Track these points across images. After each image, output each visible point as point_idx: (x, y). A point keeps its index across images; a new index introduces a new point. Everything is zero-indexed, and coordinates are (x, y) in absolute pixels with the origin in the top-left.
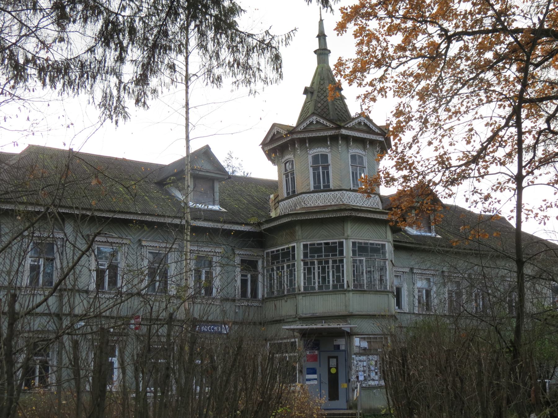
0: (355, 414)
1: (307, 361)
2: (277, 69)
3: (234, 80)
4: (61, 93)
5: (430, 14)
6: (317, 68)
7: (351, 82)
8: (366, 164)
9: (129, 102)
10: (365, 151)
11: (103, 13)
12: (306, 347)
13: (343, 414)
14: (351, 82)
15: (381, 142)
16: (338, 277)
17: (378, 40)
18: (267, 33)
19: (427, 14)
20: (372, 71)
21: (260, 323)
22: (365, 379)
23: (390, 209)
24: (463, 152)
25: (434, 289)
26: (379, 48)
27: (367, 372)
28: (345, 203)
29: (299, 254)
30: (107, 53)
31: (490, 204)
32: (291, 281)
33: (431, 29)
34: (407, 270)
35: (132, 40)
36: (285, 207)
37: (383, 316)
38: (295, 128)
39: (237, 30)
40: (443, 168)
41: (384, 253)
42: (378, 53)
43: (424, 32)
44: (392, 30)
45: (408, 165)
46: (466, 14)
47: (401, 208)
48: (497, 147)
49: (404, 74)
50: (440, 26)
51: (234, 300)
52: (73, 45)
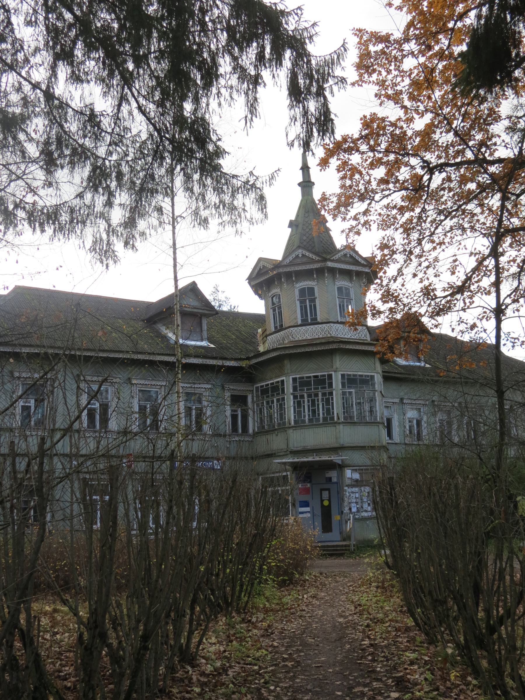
0: (349, 546)
1: (300, 493)
2: (262, 209)
3: (220, 221)
4: (52, 239)
5: (412, 147)
6: (302, 201)
7: (335, 217)
8: (352, 296)
9: (118, 246)
10: (351, 283)
11: (90, 158)
12: (298, 480)
13: (337, 546)
14: (335, 217)
15: (367, 273)
16: (328, 410)
17: (361, 173)
18: (251, 173)
19: (409, 147)
20: (355, 205)
21: (252, 458)
22: (358, 511)
23: (377, 340)
24: (448, 284)
25: (425, 418)
26: (362, 182)
27: (360, 503)
28: (333, 335)
29: (289, 388)
30: (95, 198)
31: (476, 333)
32: (281, 415)
33: (414, 161)
34: (397, 401)
35: (120, 185)
36: (273, 341)
37: (373, 448)
38: (281, 262)
39: (221, 172)
40: (428, 299)
41: (373, 385)
42: (362, 187)
43: (407, 164)
44: (375, 164)
45: (393, 297)
46: (447, 145)
47: (387, 340)
48: (482, 277)
49: (387, 207)
50: (422, 159)
51: (225, 436)
52: (62, 190)
